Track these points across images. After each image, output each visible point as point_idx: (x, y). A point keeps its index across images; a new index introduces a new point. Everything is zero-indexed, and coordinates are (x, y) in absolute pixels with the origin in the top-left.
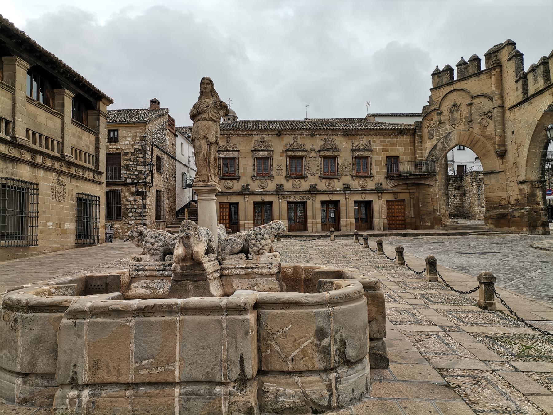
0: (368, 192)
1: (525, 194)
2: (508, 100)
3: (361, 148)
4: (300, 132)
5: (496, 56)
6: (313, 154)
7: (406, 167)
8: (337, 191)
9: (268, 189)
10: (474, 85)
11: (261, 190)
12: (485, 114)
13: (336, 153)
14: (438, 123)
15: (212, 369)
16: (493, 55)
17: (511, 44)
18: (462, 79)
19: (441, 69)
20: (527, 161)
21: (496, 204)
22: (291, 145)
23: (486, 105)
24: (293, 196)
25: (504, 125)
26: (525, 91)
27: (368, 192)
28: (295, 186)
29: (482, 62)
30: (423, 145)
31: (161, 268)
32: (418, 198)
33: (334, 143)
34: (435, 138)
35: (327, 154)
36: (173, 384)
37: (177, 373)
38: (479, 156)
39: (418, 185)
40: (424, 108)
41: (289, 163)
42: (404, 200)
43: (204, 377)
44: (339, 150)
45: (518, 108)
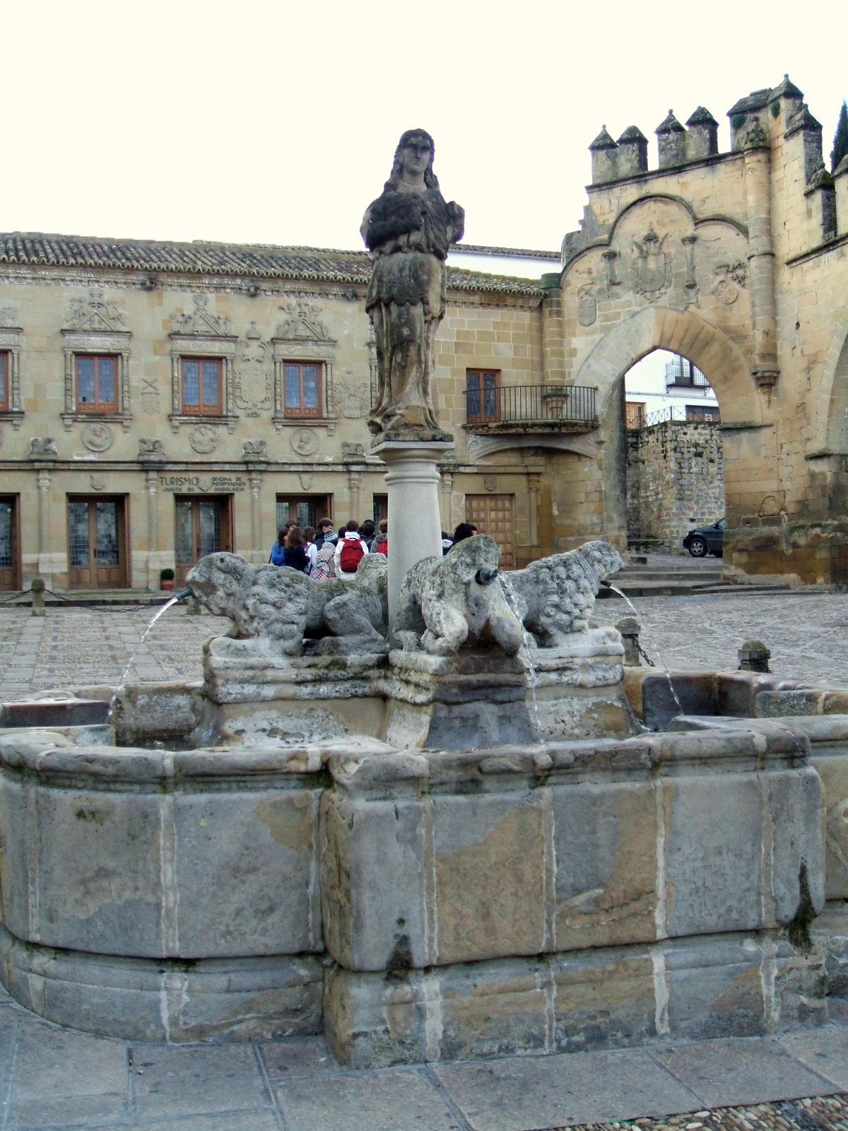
0: (315, 468)
1: (824, 487)
2: (785, 238)
4: (215, 281)
5: (757, 119)
6: (254, 350)
7: (520, 406)
9: (112, 455)
10: (696, 185)
11: (92, 457)
12: (728, 268)
14: (606, 282)
15: (740, 900)
16: (750, 116)
17: (792, 93)
18: (675, 168)
19: (615, 137)
20: (832, 401)
21: (753, 512)
22: (187, 319)
23: (728, 244)
24: (191, 475)
28: (199, 448)
29: (719, 130)
30: (566, 341)
31: (308, 674)
32: (548, 491)
33: (319, 319)
34: (597, 324)
35: (297, 352)
36: (649, 943)
37: (659, 919)
38: (714, 381)
39: (550, 453)
40: (569, 237)
41: (280, 376)
42: (512, 495)
43: (722, 920)
44: (333, 343)
45: (811, 263)
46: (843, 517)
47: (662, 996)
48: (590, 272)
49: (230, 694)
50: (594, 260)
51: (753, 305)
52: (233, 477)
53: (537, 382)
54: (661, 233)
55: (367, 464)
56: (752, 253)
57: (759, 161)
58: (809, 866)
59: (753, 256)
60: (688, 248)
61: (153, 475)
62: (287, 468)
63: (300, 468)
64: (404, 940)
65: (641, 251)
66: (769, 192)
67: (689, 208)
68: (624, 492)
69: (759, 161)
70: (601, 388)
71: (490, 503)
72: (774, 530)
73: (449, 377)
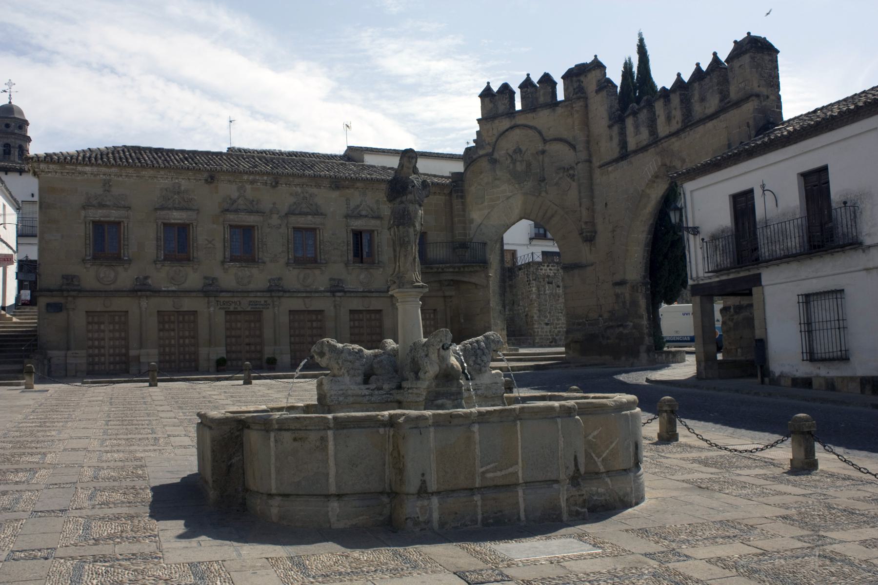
3: (364, 213)
4: (251, 177)
8: (321, 292)
9: (187, 285)
11: (174, 288)
13: (318, 220)
24: (236, 299)
25: (592, 190)
26: (623, 144)
29: (557, 86)
47: (522, 506)
52: (262, 300)
54: (524, 149)
58: (578, 455)
60: (541, 157)
61: (212, 299)
62: (295, 294)
63: (304, 295)
64: (424, 482)
65: (512, 159)
67: (540, 133)
68: (504, 306)
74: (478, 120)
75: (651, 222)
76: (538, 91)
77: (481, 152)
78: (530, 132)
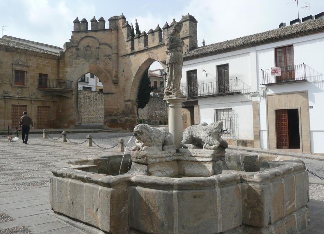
3: (20, 63)
5: (115, 22)
7: (52, 84)
12: (107, 56)
14: (76, 56)
17: (124, 18)
20: (132, 88)
23: (107, 50)
27: (24, 99)
34: (74, 65)
46: (133, 115)
48: (72, 53)
49: (150, 161)
50: (74, 50)
51: (113, 65)
53: (57, 78)
54: (91, 46)
55: (10, 97)
56: (113, 53)
57: (116, 32)
59: (113, 54)
60: (98, 50)
63: (18, 98)
65: (86, 49)
66: (118, 39)
67: (98, 40)
69: (116, 32)
70: (74, 81)
71: (43, 109)
72: (116, 118)
73: (34, 75)
74: (73, 32)
75: (141, 79)
76: (99, 24)
77: (73, 44)
78: (94, 40)
